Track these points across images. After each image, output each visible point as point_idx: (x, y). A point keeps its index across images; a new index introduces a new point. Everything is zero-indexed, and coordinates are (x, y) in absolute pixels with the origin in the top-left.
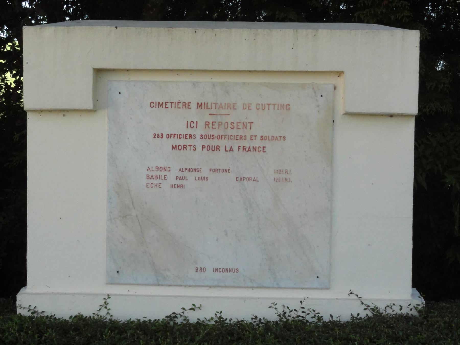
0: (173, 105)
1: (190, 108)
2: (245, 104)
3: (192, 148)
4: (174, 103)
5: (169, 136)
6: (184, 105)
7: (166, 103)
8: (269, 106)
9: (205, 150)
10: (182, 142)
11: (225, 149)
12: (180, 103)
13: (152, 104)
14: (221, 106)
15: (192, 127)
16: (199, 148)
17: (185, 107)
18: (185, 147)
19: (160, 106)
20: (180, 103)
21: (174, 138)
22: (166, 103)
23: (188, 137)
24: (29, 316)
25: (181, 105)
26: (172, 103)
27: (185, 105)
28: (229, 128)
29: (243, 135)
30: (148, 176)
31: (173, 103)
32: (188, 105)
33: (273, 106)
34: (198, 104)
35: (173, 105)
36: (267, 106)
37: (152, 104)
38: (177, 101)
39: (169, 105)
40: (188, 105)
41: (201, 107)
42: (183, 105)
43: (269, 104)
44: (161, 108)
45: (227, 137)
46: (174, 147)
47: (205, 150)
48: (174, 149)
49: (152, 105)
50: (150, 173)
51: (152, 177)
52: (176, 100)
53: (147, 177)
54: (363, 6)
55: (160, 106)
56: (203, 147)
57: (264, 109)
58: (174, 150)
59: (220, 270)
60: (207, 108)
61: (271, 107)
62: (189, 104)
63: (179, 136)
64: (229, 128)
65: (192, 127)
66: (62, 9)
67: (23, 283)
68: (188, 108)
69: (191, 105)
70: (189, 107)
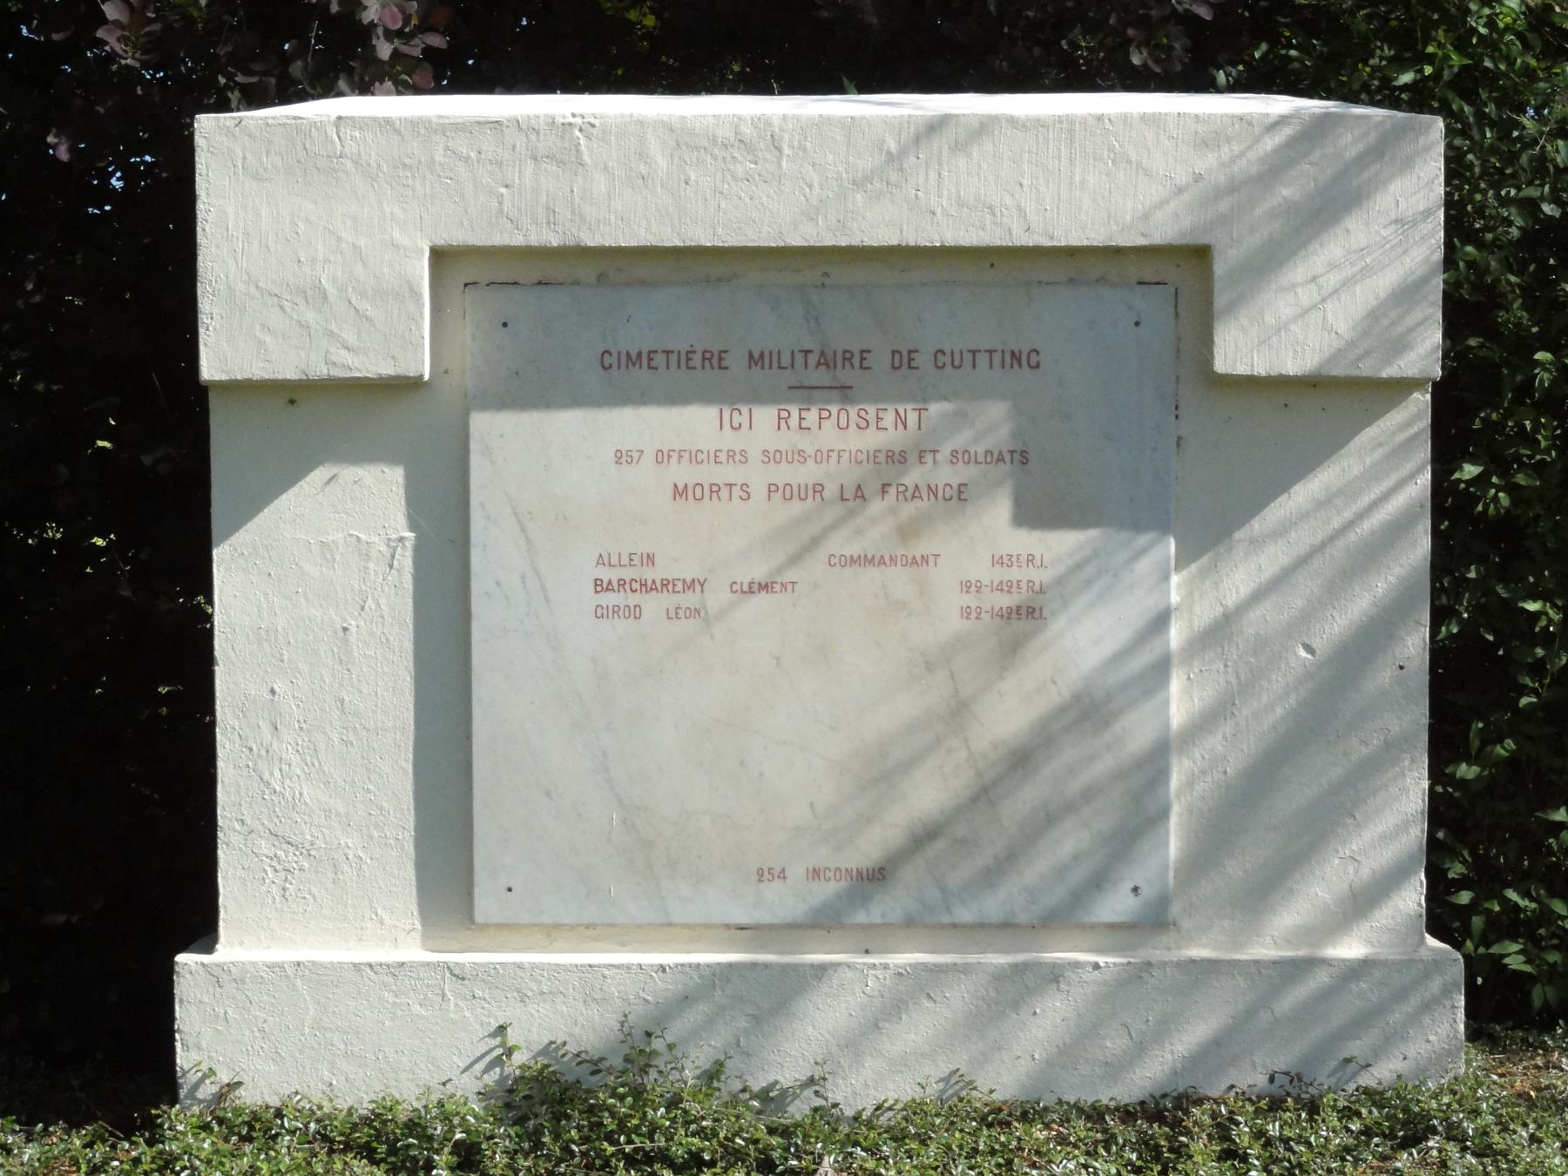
0: (673, 358)
1: (727, 368)
2: (900, 352)
3: (737, 492)
4: (675, 355)
5: (662, 457)
6: (707, 357)
7: (910, 352)
8: (806, 356)
9: (777, 497)
10: (708, 474)
11: (839, 494)
12: (695, 352)
13: (607, 358)
14: (822, 361)
15: (736, 425)
16: (759, 492)
17: (711, 364)
18: (715, 489)
19: (753, 365)
20: (695, 352)
21: (679, 462)
22: (910, 352)
23: (723, 457)
24: (1559, 809)
25: (697, 360)
26: (668, 353)
27: (710, 359)
28: (853, 426)
29: (737, 449)
30: (599, 583)
31: (809, 355)
32: (720, 359)
33: (665, 358)
34: (751, 355)
35: (673, 358)
36: (968, 357)
37: (607, 358)
38: (684, 348)
39: (659, 360)
40: (720, 359)
41: (638, 365)
42: (704, 359)
43: (974, 352)
44: (635, 371)
45: (686, 455)
46: (679, 492)
47: (777, 497)
48: (681, 495)
49: (941, 359)
50: (606, 574)
51: (609, 588)
52: (681, 345)
53: (596, 585)
54: (994, 13)
55: (753, 365)
56: (772, 489)
57: (939, 368)
58: (681, 501)
59: (828, 874)
60: (780, 368)
61: (982, 359)
62: (723, 355)
63: (695, 457)
64: (853, 426)
65: (736, 425)
66: (449, 79)
67: (202, 933)
68: (720, 367)
69: (919, 360)
70: (865, 364)
